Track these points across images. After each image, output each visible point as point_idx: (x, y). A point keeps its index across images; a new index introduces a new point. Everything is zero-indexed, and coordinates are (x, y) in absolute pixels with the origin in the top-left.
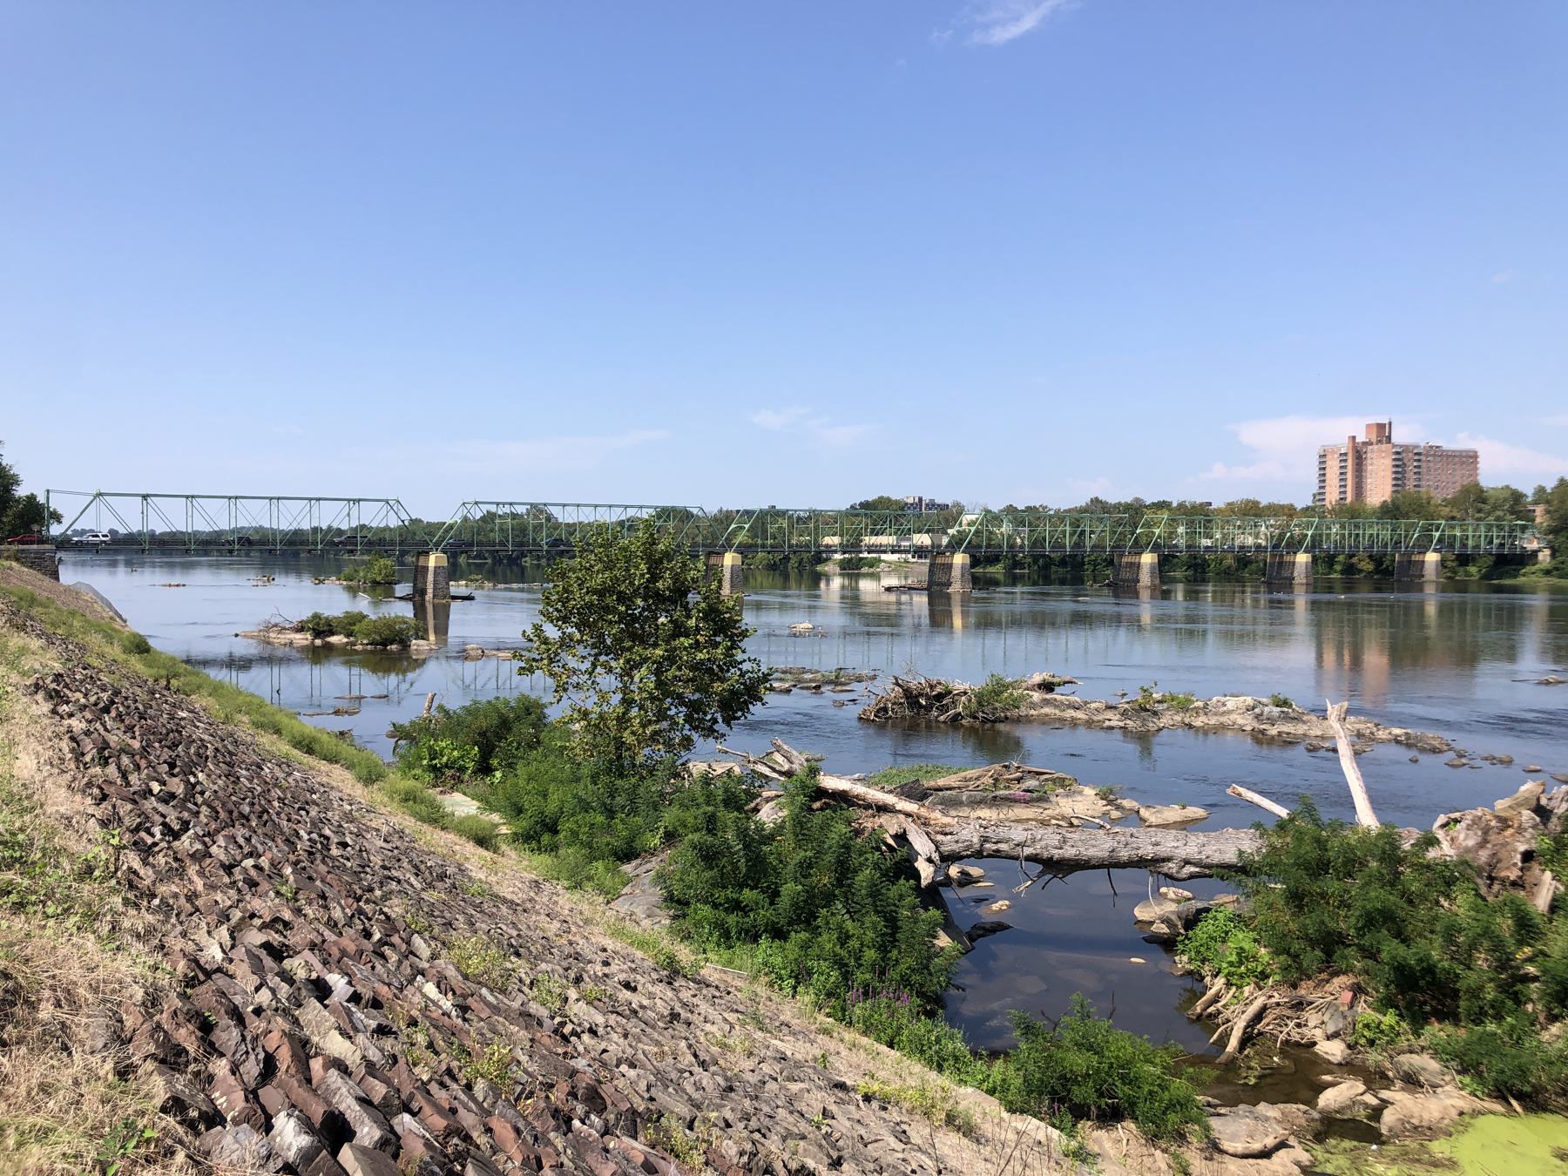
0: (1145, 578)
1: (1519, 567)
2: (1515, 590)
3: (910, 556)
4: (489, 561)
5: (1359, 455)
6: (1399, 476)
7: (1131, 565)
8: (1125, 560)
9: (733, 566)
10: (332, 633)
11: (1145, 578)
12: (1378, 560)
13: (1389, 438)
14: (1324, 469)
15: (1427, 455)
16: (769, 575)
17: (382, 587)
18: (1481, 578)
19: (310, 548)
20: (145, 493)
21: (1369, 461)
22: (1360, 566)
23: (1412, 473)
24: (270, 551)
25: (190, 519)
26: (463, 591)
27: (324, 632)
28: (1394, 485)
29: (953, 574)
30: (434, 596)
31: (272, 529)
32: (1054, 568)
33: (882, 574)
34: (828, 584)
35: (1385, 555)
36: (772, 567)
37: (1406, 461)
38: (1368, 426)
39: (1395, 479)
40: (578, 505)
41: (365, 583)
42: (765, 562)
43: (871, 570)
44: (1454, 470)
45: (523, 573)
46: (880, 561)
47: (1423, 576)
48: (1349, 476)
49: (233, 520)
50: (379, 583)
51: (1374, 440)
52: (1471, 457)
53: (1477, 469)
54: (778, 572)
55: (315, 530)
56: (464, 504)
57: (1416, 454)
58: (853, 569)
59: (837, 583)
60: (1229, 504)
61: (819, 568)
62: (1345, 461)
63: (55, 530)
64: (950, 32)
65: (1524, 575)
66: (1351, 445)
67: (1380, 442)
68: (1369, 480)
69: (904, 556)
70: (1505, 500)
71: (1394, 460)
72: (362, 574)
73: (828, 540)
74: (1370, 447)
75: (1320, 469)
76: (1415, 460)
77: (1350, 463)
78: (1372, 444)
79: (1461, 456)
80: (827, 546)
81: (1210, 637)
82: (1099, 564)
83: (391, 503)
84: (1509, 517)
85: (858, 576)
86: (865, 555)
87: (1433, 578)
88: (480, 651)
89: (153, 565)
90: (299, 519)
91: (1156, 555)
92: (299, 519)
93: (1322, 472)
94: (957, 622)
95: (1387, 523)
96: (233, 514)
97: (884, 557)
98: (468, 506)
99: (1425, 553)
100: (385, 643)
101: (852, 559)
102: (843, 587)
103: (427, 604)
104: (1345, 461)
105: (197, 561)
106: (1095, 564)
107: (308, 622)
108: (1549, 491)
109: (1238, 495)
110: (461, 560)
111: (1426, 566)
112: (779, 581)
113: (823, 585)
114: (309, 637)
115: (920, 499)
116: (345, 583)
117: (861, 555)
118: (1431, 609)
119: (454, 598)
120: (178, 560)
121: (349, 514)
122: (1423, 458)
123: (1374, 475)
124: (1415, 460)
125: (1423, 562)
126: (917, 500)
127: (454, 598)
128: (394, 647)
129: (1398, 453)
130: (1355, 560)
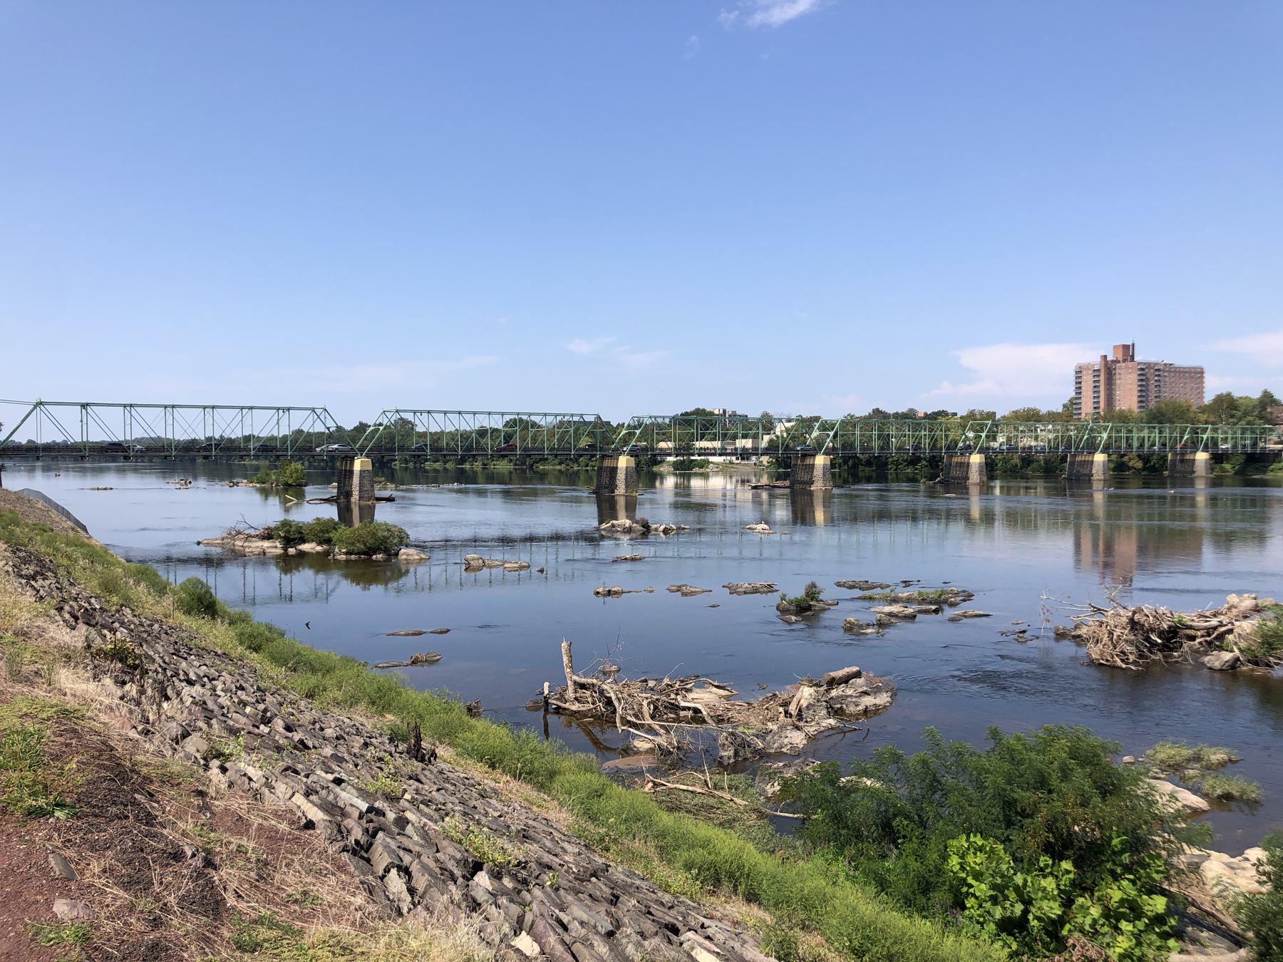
0: (974, 476)
1: (1267, 464)
2: (1264, 484)
3: (734, 458)
5: (1109, 369)
6: (1144, 388)
7: (961, 464)
8: (955, 460)
9: (627, 468)
10: (303, 541)
11: (974, 476)
12: (1145, 459)
13: (1132, 357)
14: (1080, 383)
15: (1164, 371)
17: (294, 489)
18: (1235, 474)
19: (242, 453)
20: (84, 401)
21: (1118, 376)
22: (1130, 464)
23: (1153, 386)
24: (166, 457)
25: (85, 426)
26: (386, 494)
27: (294, 539)
30: (360, 498)
31: (167, 439)
32: (861, 468)
33: (711, 474)
34: (662, 483)
35: (1152, 455)
37: (1150, 376)
38: (1115, 347)
39: (1141, 391)
40: (489, 413)
44: (1185, 384)
45: (393, 475)
46: (709, 462)
48: (1102, 389)
49: (170, 429)
50: (290, 485)
51: (1121, 359)
52: (1199, 373)
53: (1203, 382)
55: (247, 439)
57: (1156, 370)
58: (685, 469)
59: (670, 482)
60: (1013, 412)
61: (655, 469)
62: (1099, 376)
64: (737, 13)
65: (1272, 471)
66: (1103, 363)
67: (1125, 361)
69: (729, 458)
70: (1254, 407)
71: (1139, 375)
72: (274, 477)
73: (662, 445)
74: (1119, 365)
75: (1076, 383)
76: (1156, 375)
77: (1102, 378)
78: (1119, 362)
79: (1190, 372)
80: (661, 449)
82: (901, 464)
83: (318, 411)
84: (1258, 421)
85: (689, 477)
86: (696, 458)
87: (1204, 474)
88: (481, 561)
89: (67, 470)
90: (232, 426)
91: (983, 455)
92: (232, 426)
93: (1078, 386)
94: (820, 515)
95: (1154, 428)
96: (128, 422)
97: (711, 459)
98: (389, 415)
99: (1094, 453)
100: (370, 551)
101: (684, 461)
102: (677, 486)
103: (353, 506)
104: (1099, 376)
105: (105, 467)
106: (897, 463)
107: (277, 529)
109: (1021, 405)
111: (1197, 463)
113: (658, 483)
114: (278, 545)
115: (724, 411)
116: (258, 485)
117: (692, 458)
118: (1201, 499)
120: (88, 465)
122: (1161, 373)
124: (1156, 375)
126: (721, 412)
128: (380, 556)
129: (1142, 369)
130: (1126, 459)
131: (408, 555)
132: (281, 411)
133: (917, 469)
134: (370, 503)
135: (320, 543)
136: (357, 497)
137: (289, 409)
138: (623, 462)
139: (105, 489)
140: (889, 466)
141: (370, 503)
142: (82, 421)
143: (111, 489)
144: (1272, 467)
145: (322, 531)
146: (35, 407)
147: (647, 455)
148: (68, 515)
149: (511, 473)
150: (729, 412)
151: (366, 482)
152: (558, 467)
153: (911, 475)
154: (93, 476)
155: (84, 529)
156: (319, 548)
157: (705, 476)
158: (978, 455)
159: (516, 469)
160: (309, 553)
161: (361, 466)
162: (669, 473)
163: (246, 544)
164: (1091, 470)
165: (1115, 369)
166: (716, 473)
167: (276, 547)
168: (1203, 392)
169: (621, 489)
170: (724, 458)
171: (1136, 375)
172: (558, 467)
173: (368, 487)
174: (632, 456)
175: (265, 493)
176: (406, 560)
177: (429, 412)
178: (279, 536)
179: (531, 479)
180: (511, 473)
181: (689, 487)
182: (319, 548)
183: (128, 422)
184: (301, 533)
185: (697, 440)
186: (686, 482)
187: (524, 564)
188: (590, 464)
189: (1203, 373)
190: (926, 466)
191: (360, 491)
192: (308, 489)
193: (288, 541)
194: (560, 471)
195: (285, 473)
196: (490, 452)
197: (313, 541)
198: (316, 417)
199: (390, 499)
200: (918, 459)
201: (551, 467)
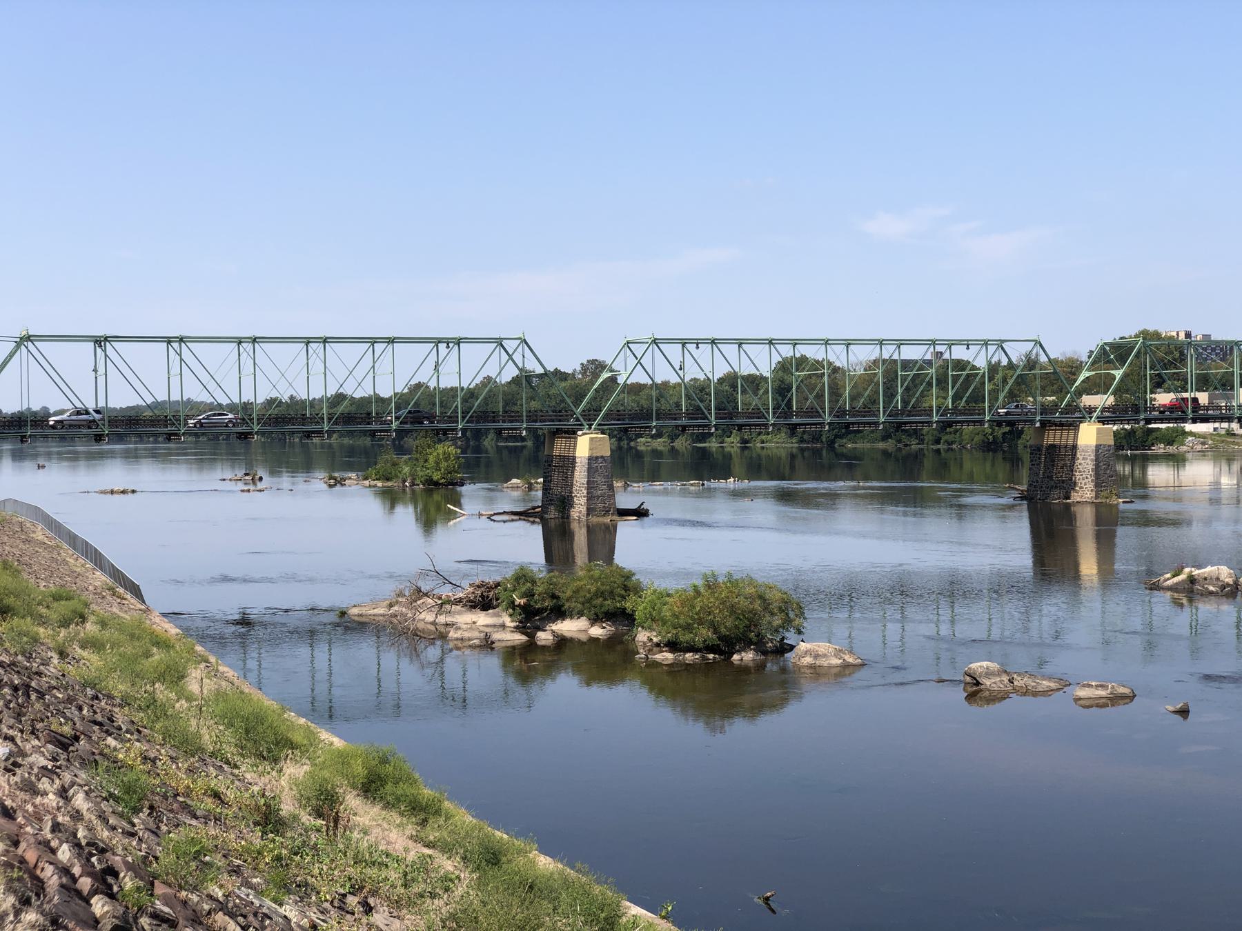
4: (529, 443)
9: (1098, 447)
10: (559, 613)
16: (985, 459)
17: (442, 491)
25: (101, 380)
30: (590, 511)
33: (1189, 456)
36: (990, 447)
41: (413, 484)
42: (977, 439)
43: (1172, 449)
46: (1185, 434)
49: (175, 381)
50: (437, 484)
54: (1000, 455)
63: (618, 484)
69: (1225, 425)
72: (406, 469)
85: (1146, 460)
89: (49, 455)
96: (175, 369)
100: (726, 645)
101: (1133, 431)
103: (575, 526)
110: (486, 443)
112: (1002, 469)
116: (380, 484)
119: (624, 513)
120: (80, 449)
121: (373, 367)
127: (624, 513)
128: (747, 657)
131: (816, 656)
132: (442, 346)
134: (607, 520)
135: (595, 620)
136: (584, 510)
137: (458, 342)
138: (1089, 435)
139: (124, 492)
141: (607, 520)
142: (95, 370)
143: (133, 491)
145: (600, 594)
146: (19, 345)
148: (97, 559)
149: (793, 457)
150: (585, 362)
152: (881, 445)
154: (88, 466)
155: (136, 591)
156: (597, 631)
157: (1178, 460)
159: (802, 450)
160: (571, 640)
163: (442, 619)
166: (1203, 454)
167: (503, 626)
169: (1085, 491)
170: (1217, 425)
172: (881, 445)
173: (602, 490)
175: (391, 498)
176: (812, 667)
177: (713, 342)
178: (512, 605)
179: (831, 467)
182: (597, 631)
183: (175, 369)
184: (554, 597)
186: (1137, 472)
187: (1122, 690)
188: (944, 439)
191: (590, 498)
192: (466, 489)
193: (531, 617)
194: (885, 453)
195: (426, 461)
196: (828, 419)
197: (580, 614)
198: (505, 357)
199: (640, 513)
201: (868, 445)
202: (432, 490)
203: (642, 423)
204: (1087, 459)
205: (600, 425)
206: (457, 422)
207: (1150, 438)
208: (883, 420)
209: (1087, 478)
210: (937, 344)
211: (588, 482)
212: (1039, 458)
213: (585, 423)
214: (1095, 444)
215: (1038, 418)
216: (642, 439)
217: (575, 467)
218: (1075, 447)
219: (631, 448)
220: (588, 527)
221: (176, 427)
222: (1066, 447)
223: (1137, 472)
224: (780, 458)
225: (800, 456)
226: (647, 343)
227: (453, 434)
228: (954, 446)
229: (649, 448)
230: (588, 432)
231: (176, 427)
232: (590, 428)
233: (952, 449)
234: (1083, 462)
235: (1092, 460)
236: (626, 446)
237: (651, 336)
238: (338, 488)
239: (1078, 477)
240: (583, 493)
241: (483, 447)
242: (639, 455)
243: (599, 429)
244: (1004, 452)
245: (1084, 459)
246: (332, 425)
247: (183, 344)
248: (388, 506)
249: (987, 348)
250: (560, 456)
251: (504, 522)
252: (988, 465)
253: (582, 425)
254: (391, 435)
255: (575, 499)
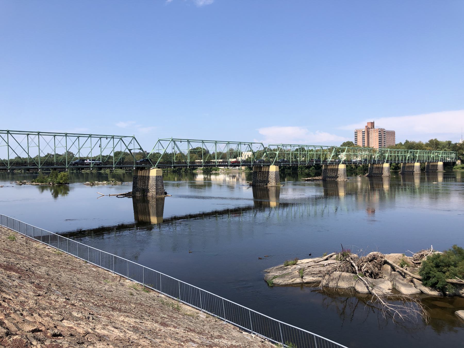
0: (386, 173)
6: (381, 138)
9: (276, 171)
11: (386, 173)
23: (383, 138)
28: (379, 141)
29: (339, 173)
32: (286, 170)
39: (380, 139)
43: (217, 172)
44: (390, 137)
47: (437, 170)
50: (61, 184)
53: (395, 137)
56: (159, 140)
57: (384, 132)
66: (366, 129)
67: (372, 128)
68: (371, 140)
70: (447, 145)
75: (355, 136)
76: (384, 134)
77: (366, 134)
79: (391, 133)
81: (377, 190)
82: (303, 168)
85: (211, 175)
93: (356, 137)
103: (150, 199)
104: (364, 134)
108: (403, 144)
123: (372, 138)
124: (384, 134)
125: (437, 165)
129: (380, 131)
133: (310, 170)
140: (298, 169)
144: (454, 167)
147: (171, 167)
151: (159, 183)
153: (307, 173)
158: (275, 166)
159: (126, 172)
161: (276, 170)
162: (201, 173)
164: (413, 169)
165: (369, 131)
168: (395, 140)
171: (378, 133)
174: (159, 168)
180: (124, 174)
181: (210, 180)
185: (240, 157)
186: (209, 177)
189: (395, 133)
190: (314, 169)
200: (311, 167)
202: (60, 186)
203: (168, 165)
204: (273, 175)
205: (157, 166)
206: (251, 163)
207: (212, 169)
208: (67, 167)
209: (273, 180)
210: (68, 136)
211: (156, 184)
212: (256, 175)
213: (153, 165)
214: (275, 171)
215: (262, 164)
216: (83, 170)
217: (149, 179)
218: (268, 172)
219: (80, 172)
220: (156, 199)
221: (6, 166)
222: (265, 172)
223: (209, 177)
224: (120, 175)
225: (126, 174)
226: (170, 141)
227: (36, 170)
228: (165, 171)
229: (85, 172)
230: (154, 168)
231: (6, 166)
232: (154, 167)
233: (165, 172)
234: (271, 176)
235: (274, 175)
236: (79, 172)
237: (171, 138)
238: (23, 185)
239: (270, 180)
240: (154, 188)
241: (38, 173)
242: (82, 174)
243: (157, 167)
244: (177, 173)
245: (271, 175)
246: (69, 165)
247: (9, 135)
248: (41, 190)
249: (241, 145)
250: (141, 176)
251: (121, 197)
252: (174, 176)
253: (152, 166)
254: (7, 171)
255: (150, 190)
